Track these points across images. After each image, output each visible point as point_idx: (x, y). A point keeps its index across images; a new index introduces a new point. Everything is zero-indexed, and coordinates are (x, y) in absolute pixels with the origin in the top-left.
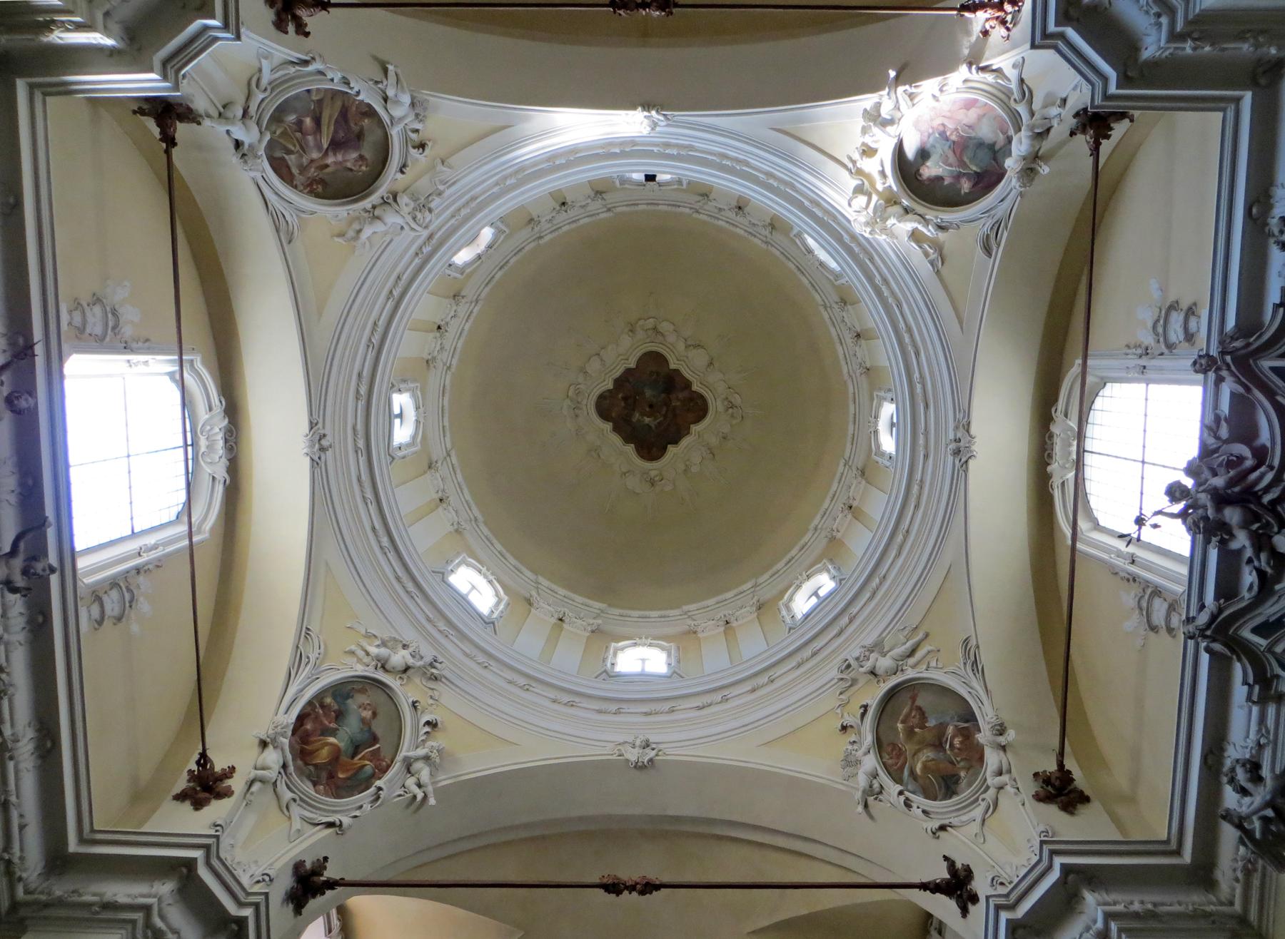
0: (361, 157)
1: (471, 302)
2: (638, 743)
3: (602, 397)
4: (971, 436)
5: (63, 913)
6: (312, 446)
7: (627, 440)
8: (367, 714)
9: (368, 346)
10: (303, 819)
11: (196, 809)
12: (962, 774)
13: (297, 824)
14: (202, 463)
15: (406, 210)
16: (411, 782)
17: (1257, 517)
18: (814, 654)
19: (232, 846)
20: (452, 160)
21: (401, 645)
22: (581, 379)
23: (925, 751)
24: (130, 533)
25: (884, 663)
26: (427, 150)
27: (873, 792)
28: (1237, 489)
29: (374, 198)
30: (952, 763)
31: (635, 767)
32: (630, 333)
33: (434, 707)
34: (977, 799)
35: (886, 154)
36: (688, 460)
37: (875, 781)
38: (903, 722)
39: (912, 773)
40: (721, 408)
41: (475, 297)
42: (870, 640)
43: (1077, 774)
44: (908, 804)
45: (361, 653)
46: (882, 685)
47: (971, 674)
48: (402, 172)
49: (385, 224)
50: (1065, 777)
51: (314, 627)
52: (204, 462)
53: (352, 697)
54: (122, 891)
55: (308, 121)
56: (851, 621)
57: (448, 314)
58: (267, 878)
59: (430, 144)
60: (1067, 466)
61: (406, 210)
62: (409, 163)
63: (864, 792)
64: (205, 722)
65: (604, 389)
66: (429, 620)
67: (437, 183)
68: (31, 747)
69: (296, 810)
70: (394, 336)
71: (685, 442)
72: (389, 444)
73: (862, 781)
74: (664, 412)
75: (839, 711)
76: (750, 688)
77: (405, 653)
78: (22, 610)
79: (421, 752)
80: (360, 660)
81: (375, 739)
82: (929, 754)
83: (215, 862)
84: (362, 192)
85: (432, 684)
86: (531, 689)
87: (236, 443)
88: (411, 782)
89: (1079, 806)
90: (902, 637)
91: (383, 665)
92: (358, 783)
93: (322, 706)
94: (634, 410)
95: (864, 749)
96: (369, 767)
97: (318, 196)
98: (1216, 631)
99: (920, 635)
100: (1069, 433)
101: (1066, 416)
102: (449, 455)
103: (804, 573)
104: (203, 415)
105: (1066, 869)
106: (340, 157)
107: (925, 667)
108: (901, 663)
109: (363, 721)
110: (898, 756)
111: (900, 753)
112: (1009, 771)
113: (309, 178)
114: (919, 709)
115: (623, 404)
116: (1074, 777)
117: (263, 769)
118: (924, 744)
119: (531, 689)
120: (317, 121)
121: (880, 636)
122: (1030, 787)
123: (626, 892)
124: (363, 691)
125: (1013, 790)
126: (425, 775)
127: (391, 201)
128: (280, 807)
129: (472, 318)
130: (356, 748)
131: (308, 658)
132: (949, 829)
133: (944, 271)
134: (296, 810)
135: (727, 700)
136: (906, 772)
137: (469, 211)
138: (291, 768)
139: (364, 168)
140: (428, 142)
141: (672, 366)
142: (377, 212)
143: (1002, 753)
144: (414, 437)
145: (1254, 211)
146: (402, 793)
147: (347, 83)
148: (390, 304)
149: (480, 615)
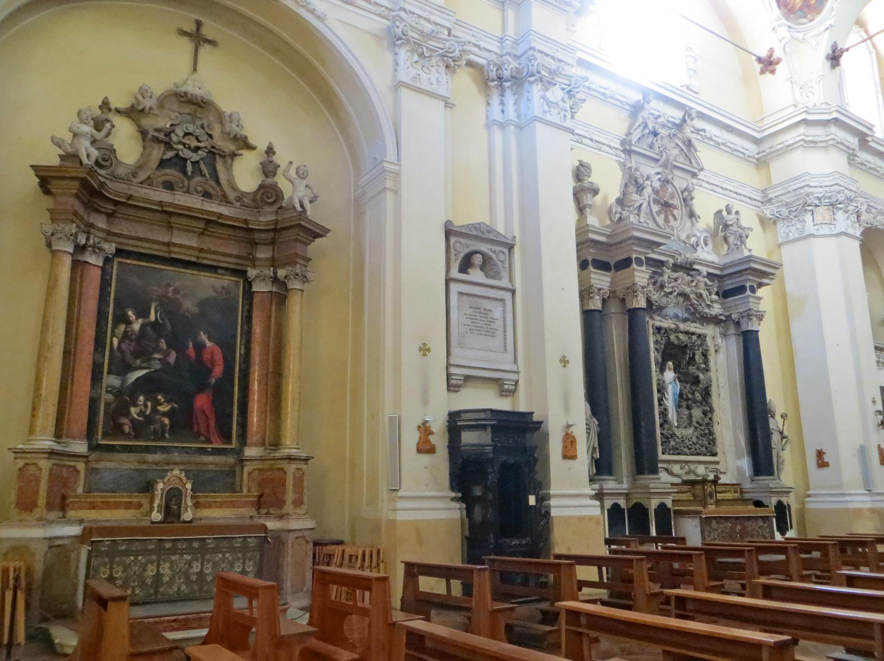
54: (790, 138)
64: (747, 49)
117: (783, 38)
138: (793, 25)
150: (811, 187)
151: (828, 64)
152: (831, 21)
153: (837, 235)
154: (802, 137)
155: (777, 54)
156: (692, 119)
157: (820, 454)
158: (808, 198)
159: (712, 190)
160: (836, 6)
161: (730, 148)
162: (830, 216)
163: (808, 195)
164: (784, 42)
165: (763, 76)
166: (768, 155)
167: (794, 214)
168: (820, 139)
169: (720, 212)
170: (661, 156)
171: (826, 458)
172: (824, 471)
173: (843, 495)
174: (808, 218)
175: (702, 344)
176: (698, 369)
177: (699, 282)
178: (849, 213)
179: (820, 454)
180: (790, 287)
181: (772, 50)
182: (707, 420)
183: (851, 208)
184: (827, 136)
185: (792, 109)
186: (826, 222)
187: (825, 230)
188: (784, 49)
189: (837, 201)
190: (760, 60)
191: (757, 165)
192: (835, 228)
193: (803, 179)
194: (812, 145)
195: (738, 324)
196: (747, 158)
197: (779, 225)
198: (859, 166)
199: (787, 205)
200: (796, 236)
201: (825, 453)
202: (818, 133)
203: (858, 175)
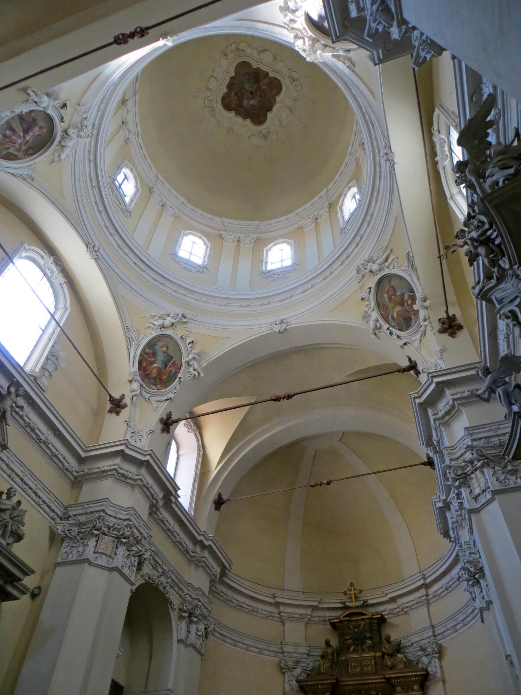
0: (41, 127)
1: (133, 96)
2: (278, 323)
3: (224, 98)
4: (392, 153)
5: (91, 476)
6: (91, 253)
7: (245, 117)
8: (164, 349)
9: (93, 188)
10: (156, 401)
11: (118, 415)
12: (413, 317)
13: (155, 405)
14: (53, 280)
15: (74, 136)
16: (191, 369)
17: (492, 251)
18: (348, 257)
19: (135, 425)
20: (82, 102)
21: (166, 316)
22: (208, 93)
23: (397, 307)
24: (42, 332)
25: (375, 267)
26: (68, 105)
27: (377, 329)
28: (483, 238)
29: (58, 139)
30: (408, 312)
31: (279, 333)
32: (225, 57)
33: (190, 334)
34: (418, 330)
35: (301, 23)
36: (280, 118)
37: (377, 323)
38: (387, 293)
39: (393, 318)
40: (288, 83)
41: (133, 92)
42: (366, 257)
43: (459, 315)
44: (391, 333)
45: (152, 326)
46: (376, 276)
47: (411, 271)
48: (63, 122)
49: (69, 147)
51: (129, 324)
52: (53, 279)
53: (156, 345)
54: (106, 465)
55: (8, 132)
56: (361, 238)
57: (124, 113)
58: (151, 431)
59: (67, 102)
60: (444, 158)
61: (74, 136)
62: (64, 115)
63: (373, 330)
64: (106, 387)
65: (223, 94)
66: (175, 291)
67: (82, 115)
68: (53, 436)
69: (153, 399)
70: (100, 161)
71: (275, 108)
72: (124, 204)
73: (372, 324)
74: (259, 95)
75: (359, 291)
76: (322, 278)
77: (169, 319)
78: (24, 402)
79: (191, 356)
80: (153, 329)
81: (171, 358)
82: (399, 308)
83: (130, 446)
84: (51, 137)
85: (185, 326)
86: (229, 304)
87: (61, 262)
88: (191, 369)
89: (458, 332)
90: (381, 253)
91: (163, 327)
92: (172, 377)
93: (146, 354)
94: (243, 99)
95: (371, 310)
96: (173, 370)
97: (32, 155)
98: (482, 296)
99: (388, 252)
100: (442, 140)
101: (439, 132)
102: (157, 178)
103: (347, 187)
104: (42, 262)
105: (438, 384)
106: (31, 134)
107: (392, 267)
108: (382, 265)
109: (164, 352)
111: (387, 308)
112: (429, 318)
113: (24, 151)
114: (392, 287)
115: (236, 98)
116: (457, 317)
117: (134, 391)
118: (396, 304)
119: (229, 304)
120: (12, 129)
121: (370, 255)
122: (437, 326)
123: (282, 400)
124: (159, 340)
125: (430, 328)
126: (196, 365)
127: (65, 136)
129: (137, 103)
130: (166, 364)
131: (132, 338)
132: (408, 344)
133: (356, 70)
134: (153, 399)
135: (314, 286)
136: (390, 317)
137: (104, 104)
138: (144, 385)
139: (44, 130)
140: (66, 102)
141: (254, 67)
142: (62, 144)
143: (426, 310)
144: (136, 187)
145: (474, 99)
146: (189, 375)
147: (13, 112)
148: (92, 165)
149: (199, 266)
151: (160, 426)
152: (172, 396)
153: (111, 570)
156: (17, 396)
158: (98, 522)
159: (9, 476)
160: (178, 387)
161: (50, 450)
162: (113, 548)
164: (134, 393)
165: (110, 414)
166: (85, 475)
167: (81, 535)
168: (131, 476)
174: (92, 542)
178: (132, 553)
180: (45, 616)
183: (134, 549)
184: (137, 475)
186: (106, 552)
187: (102, 561)
188: (132, 398)
189: (122, 535)
190: (112, 400)
192: (112, 562)
193: (102, 503)
194: (122, 479)
198: (160, 522)
199: (79, 525)
200: (75, 558)
202: (130, 469)
203: (152, 524)
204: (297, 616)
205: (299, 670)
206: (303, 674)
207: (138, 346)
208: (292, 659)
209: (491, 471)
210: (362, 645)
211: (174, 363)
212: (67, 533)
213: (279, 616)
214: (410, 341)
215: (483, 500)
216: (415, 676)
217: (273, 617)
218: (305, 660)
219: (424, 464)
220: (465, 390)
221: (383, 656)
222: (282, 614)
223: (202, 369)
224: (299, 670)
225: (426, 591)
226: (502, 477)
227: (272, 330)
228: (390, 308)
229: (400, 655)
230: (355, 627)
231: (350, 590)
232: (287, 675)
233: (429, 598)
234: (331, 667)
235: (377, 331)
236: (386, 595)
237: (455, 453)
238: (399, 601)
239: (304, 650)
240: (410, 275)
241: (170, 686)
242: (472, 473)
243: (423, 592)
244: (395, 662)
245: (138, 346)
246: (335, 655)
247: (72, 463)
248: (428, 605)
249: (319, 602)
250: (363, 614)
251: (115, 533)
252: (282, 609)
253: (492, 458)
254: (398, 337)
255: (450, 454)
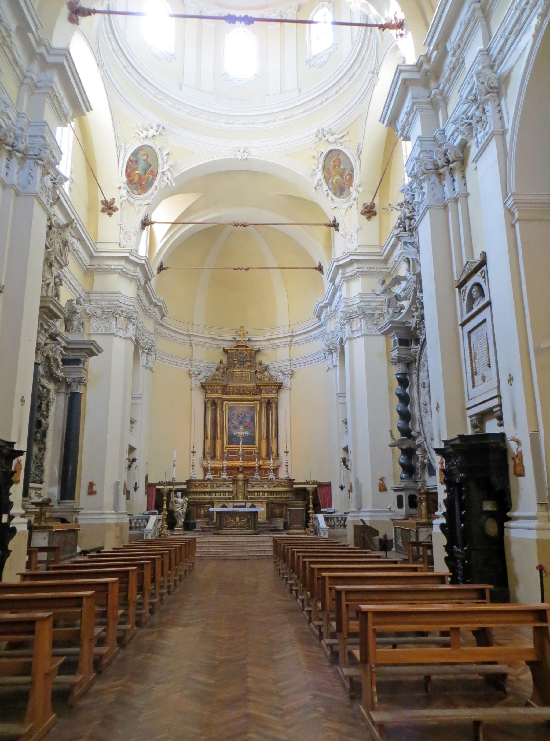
8: (145, 157)
10: (138, 205)
12: (346, 189)
16: (165, 178)
27: (319, 185)
38: (333, 162)
39: (332, 182)
44: (328, 195)
45: (137, 135)
50: (372, 206)
54: (114, 264)
69: (136, 203)
81: (150, 166)
99: (346, 133)
107: (344, 145)
110: (329, 174)
117: (123, 197)
122: (361, 208)
126: (169, 175)
128: (131, 204)
134: (136, 203)
150: (119, 302)
152: (149, 201)
153: (127, 339)
154: (122, 267)
155: (116, 204)
157: (91, 485)
160: (155, 193)
163: (119, 307)
164: (123, 199)
166: (96, 269)
167: (105, 316)
168: (130, 273)
169: (71, 300)
170: (51, 246)
171: (95, 488)
172: (92, 497)
173: (103, 514)
175: (47, 397)
176: (42, 415)
177: (57, 349)
179: (91, 485)
181: (113, 200)
182: (40, 456)
184: (134, 272)
185: (116, 246)
187: (121, 333)
189: (131, 317)
191: (85, 272)
193: (117, 295)
194: (124, 274)
195: (68, 386)
196: (83, 266)
197: (93, 320)
200: (104, 331)
201: (95, 485)
202: (130, 268)
204: (202, 343)
205: (201, 376)
206: (203, 378)
207: (125, 155)
208: (198, 369)
209: (365, 322)
210: (243, 365)
211: (152, 171)
212: (93, 312)
213: (189, 342)
214: (339, 207)
215: (356, 334)
216: (275, 386)
217: (185, 343)
218: (205, 370)
219: (316, 269)
220: (365, 267)
221: (256, 372)
222: (192, 342)
223: (174, 179)
224: (201, 376)
225: (291, 339)
226: (370, 327)
227: (235, 155)
228: (333, 175)
229: (266, 373)
230: (240, 353)
231: (240, 331)
232: (193, 379)
233: (292, 343)
234: (222, 376)
235: (318, 188)
236: (264, 337)
237: (348, 303)
238: (272, 342)
239: (206, 365)
240: (356, 161)
241: (140, 392)
242: (355, 317)
243: (289, 339)
244: (263, 377)
245: (125, 155)
246: (226, 369)
247: (87, 260)
248: (290, 346)
249: (218, 336)
250: (247, 347)
251: (125, 314)
252: (192, 338)
253: (368, 315)
254: (332, 199)
255: (346, 303)
